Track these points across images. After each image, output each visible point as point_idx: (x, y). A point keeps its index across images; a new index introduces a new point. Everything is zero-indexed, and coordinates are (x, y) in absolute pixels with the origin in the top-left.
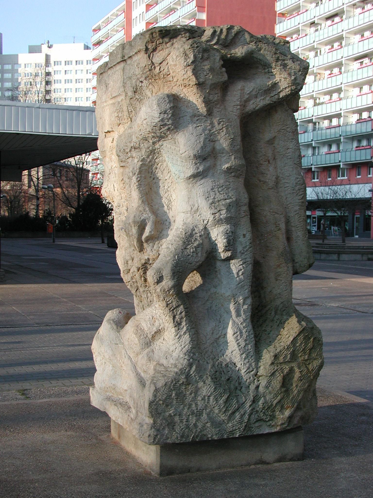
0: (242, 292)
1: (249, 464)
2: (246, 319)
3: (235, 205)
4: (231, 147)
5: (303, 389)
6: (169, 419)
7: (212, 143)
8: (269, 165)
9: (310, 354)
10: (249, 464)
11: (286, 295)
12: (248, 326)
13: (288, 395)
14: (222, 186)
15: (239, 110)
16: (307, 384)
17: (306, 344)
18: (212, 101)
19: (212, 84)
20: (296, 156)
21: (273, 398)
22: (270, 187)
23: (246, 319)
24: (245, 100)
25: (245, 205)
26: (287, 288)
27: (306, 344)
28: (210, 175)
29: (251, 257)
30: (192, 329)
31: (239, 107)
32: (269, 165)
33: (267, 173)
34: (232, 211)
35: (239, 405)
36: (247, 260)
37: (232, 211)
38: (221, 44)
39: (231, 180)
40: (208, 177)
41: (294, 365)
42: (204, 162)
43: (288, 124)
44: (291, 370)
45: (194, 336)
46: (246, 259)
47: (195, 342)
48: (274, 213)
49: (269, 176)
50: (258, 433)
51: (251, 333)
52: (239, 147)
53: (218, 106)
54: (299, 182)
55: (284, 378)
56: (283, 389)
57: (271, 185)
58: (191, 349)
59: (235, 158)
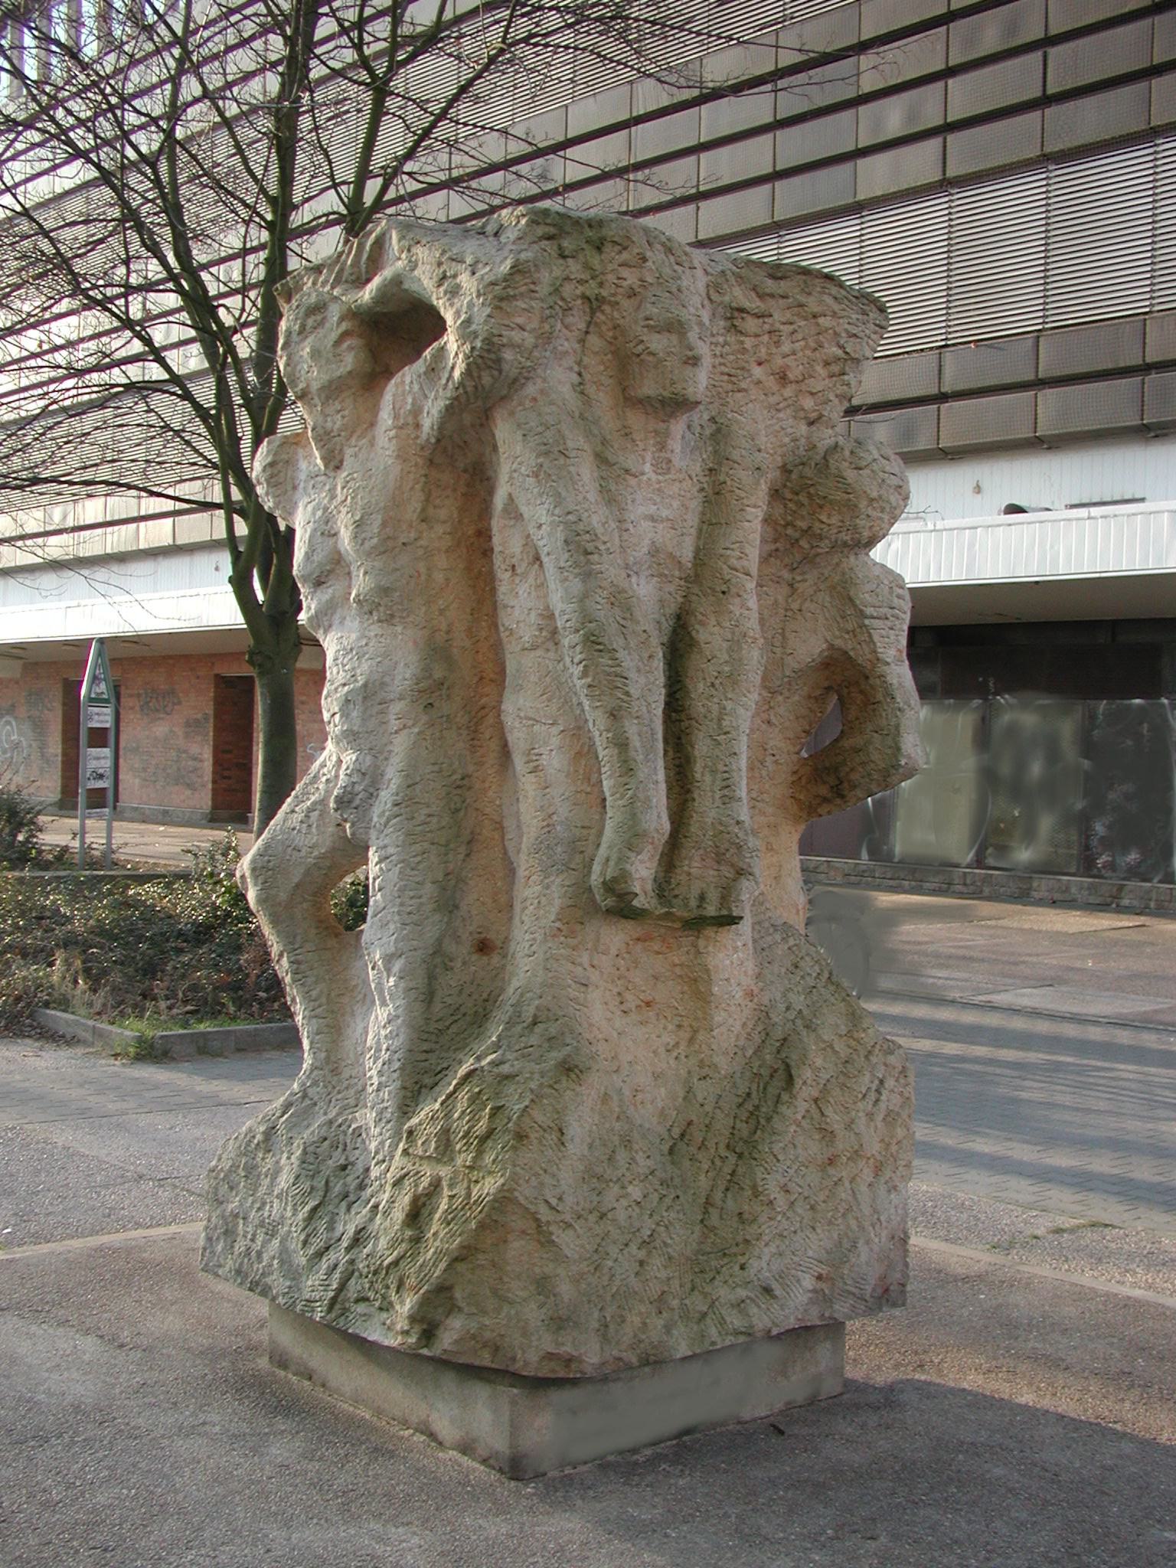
0: (384, 940)
1: (405, 1423)
2: (397, 1017)
3: (360, 698)
4: (356, 543)
5: (447, 1249)
6: (589, 1284)
7: (332, 541)
8: (517, 580)
9: (480, 1153)
10: (405, 1423)
11: (526, 969)
12: (397, 1035)
13: (414, 1257)
14: (351, 650)
15: (394, 441)
16: (459, 1240)
17: (474, 1120)
18: (332, 431)
19: (322, 389)
20: (559, 544)
21: (388, 1249)
22: (527, 645)
23: (397, 1017)
24: (410, 411)
25: (400, 699)
26: (534, 948)
27: (474, 1120)
28: (337, 622)
29: (399, 843)
30: (314, 1020)
31: (392, 433)
32: (517, 582)
33: (511, 604)
34: (355, 714)
35: (330, 1239)
36: (391, 850)
37: (355, 714)
38: (346, 281)
39: (375, 629)
40: (334, 628)
41: (444, 1171)
42: (319, 592)
43: (518, 453)
44: (436, 1185)
45: (318, 1037)
46: (385, 847)
47: (323, 1055)
48: (531, 722)
49: (517, 613)
50: (357, 1331)
51: (396, 1056)
52: (375, 540)
53: (353, 441)
54: (568, 624)
55: (415, 1200)
56: (409, 1233)
57: (526, 638)
58: (312, 1071)
59: (366, 573)
